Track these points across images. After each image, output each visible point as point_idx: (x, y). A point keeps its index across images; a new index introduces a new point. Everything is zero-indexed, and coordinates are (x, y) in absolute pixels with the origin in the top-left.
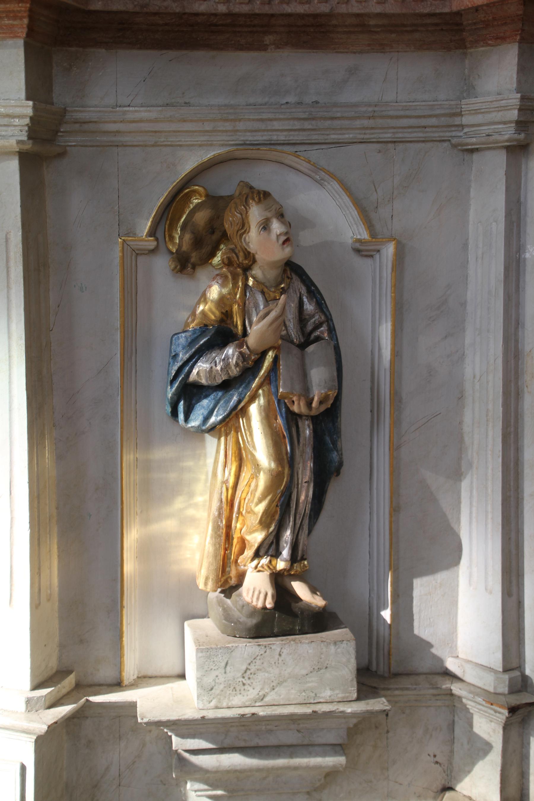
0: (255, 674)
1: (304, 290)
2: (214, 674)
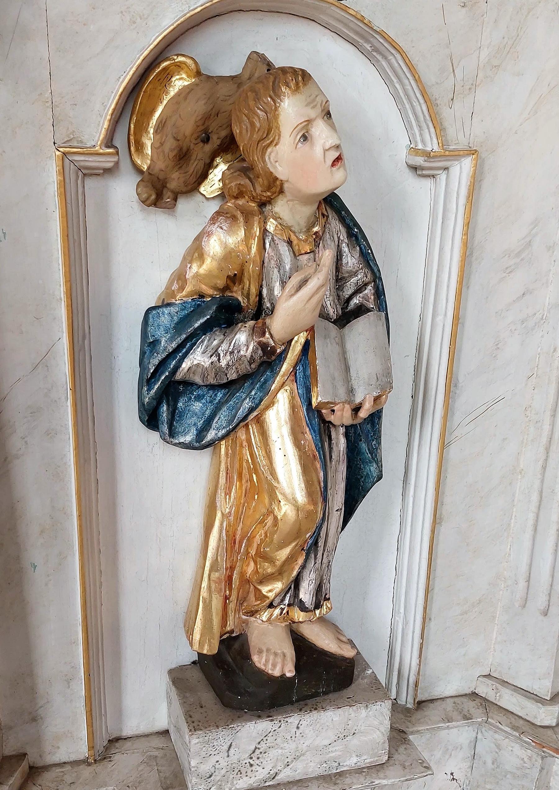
0: (265, 753)
1: (343, 236)
2: (213, 759)
